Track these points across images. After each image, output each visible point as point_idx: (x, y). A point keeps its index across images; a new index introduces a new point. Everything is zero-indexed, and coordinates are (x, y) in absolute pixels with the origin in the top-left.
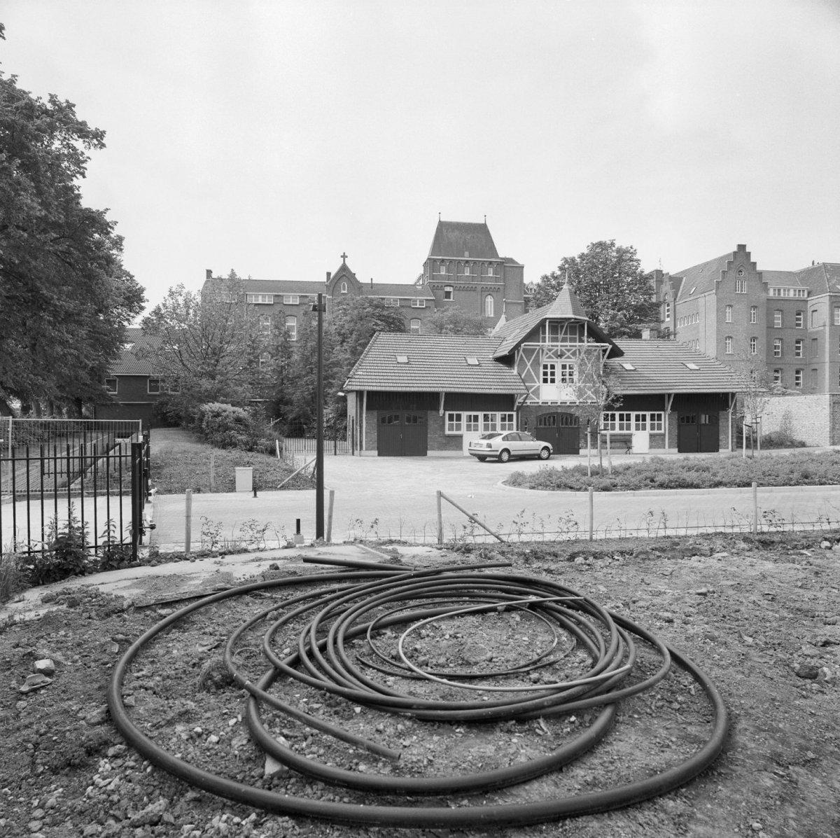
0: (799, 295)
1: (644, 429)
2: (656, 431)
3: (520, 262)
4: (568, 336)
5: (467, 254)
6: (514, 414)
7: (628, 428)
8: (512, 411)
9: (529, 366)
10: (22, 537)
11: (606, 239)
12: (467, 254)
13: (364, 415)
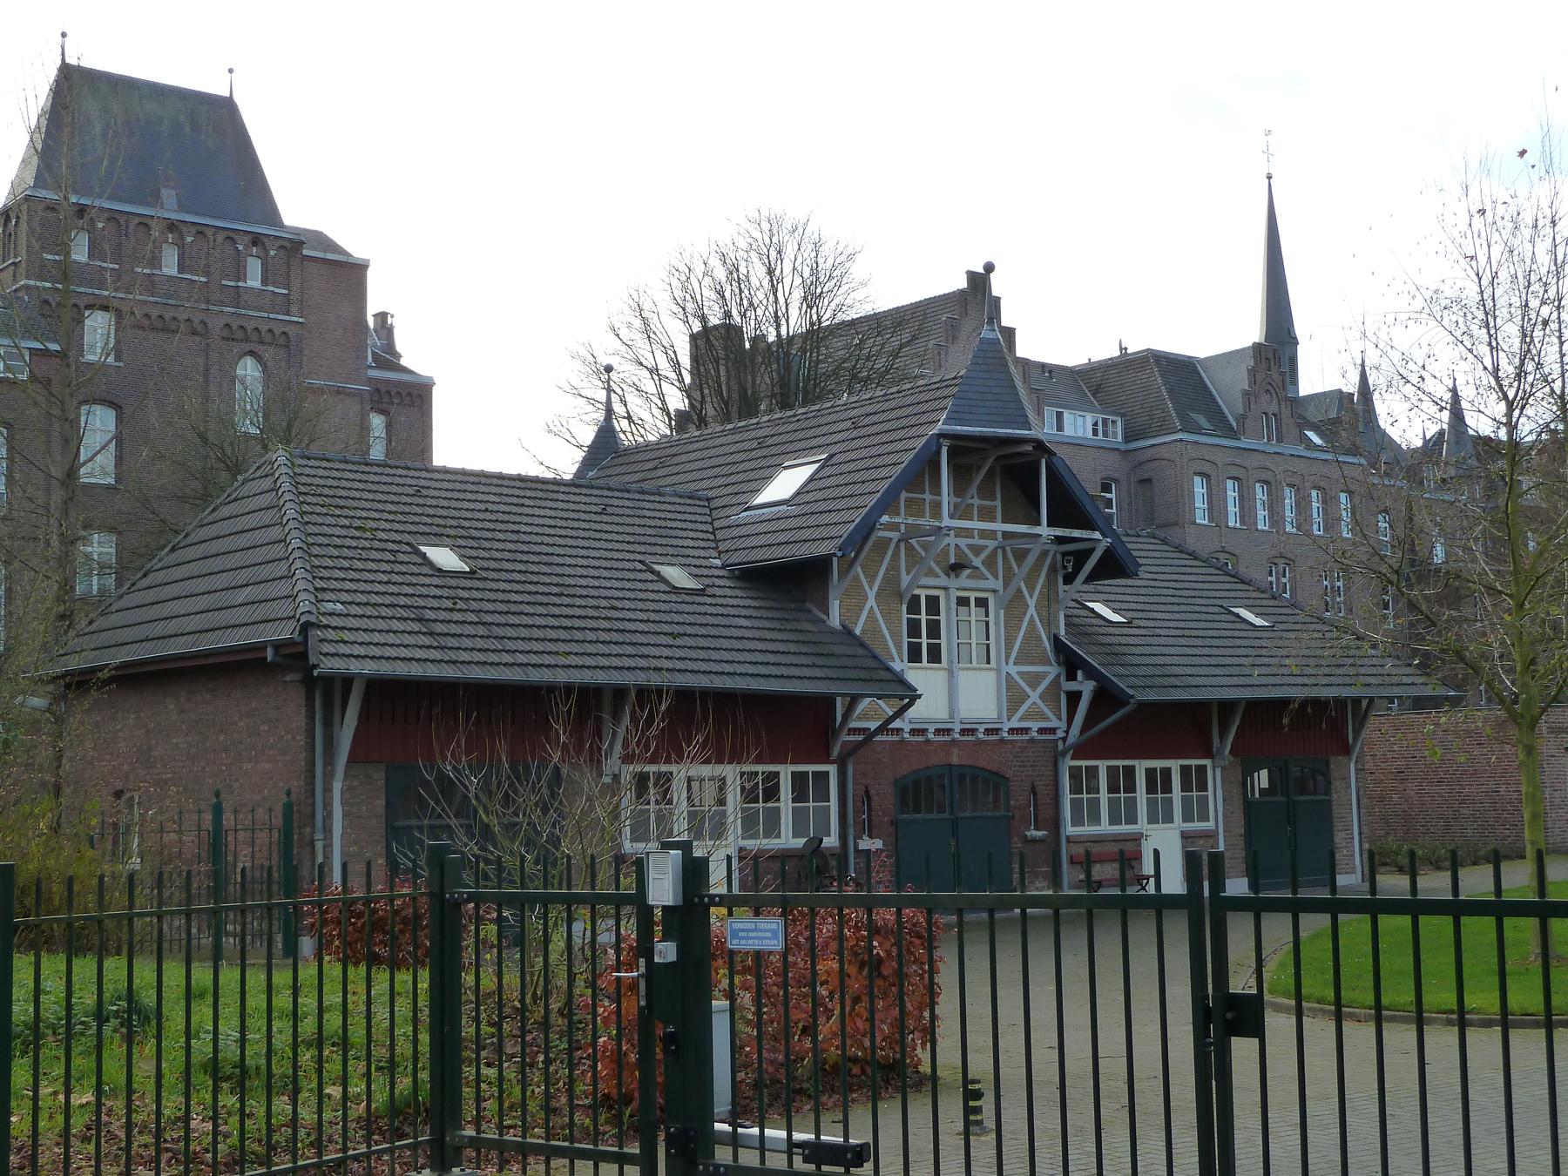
0: (1105, 434)
1: (1169, 819)
3: (355, 247)
4: (976, 502)
5: (169, 196)
6: (832, 769)
7: (1132, 819)
8: (826, 760)
9: (871, 602)
10: (1075, 964)
11: (793, 213)
12: (169, 196)
13: (337, 787)
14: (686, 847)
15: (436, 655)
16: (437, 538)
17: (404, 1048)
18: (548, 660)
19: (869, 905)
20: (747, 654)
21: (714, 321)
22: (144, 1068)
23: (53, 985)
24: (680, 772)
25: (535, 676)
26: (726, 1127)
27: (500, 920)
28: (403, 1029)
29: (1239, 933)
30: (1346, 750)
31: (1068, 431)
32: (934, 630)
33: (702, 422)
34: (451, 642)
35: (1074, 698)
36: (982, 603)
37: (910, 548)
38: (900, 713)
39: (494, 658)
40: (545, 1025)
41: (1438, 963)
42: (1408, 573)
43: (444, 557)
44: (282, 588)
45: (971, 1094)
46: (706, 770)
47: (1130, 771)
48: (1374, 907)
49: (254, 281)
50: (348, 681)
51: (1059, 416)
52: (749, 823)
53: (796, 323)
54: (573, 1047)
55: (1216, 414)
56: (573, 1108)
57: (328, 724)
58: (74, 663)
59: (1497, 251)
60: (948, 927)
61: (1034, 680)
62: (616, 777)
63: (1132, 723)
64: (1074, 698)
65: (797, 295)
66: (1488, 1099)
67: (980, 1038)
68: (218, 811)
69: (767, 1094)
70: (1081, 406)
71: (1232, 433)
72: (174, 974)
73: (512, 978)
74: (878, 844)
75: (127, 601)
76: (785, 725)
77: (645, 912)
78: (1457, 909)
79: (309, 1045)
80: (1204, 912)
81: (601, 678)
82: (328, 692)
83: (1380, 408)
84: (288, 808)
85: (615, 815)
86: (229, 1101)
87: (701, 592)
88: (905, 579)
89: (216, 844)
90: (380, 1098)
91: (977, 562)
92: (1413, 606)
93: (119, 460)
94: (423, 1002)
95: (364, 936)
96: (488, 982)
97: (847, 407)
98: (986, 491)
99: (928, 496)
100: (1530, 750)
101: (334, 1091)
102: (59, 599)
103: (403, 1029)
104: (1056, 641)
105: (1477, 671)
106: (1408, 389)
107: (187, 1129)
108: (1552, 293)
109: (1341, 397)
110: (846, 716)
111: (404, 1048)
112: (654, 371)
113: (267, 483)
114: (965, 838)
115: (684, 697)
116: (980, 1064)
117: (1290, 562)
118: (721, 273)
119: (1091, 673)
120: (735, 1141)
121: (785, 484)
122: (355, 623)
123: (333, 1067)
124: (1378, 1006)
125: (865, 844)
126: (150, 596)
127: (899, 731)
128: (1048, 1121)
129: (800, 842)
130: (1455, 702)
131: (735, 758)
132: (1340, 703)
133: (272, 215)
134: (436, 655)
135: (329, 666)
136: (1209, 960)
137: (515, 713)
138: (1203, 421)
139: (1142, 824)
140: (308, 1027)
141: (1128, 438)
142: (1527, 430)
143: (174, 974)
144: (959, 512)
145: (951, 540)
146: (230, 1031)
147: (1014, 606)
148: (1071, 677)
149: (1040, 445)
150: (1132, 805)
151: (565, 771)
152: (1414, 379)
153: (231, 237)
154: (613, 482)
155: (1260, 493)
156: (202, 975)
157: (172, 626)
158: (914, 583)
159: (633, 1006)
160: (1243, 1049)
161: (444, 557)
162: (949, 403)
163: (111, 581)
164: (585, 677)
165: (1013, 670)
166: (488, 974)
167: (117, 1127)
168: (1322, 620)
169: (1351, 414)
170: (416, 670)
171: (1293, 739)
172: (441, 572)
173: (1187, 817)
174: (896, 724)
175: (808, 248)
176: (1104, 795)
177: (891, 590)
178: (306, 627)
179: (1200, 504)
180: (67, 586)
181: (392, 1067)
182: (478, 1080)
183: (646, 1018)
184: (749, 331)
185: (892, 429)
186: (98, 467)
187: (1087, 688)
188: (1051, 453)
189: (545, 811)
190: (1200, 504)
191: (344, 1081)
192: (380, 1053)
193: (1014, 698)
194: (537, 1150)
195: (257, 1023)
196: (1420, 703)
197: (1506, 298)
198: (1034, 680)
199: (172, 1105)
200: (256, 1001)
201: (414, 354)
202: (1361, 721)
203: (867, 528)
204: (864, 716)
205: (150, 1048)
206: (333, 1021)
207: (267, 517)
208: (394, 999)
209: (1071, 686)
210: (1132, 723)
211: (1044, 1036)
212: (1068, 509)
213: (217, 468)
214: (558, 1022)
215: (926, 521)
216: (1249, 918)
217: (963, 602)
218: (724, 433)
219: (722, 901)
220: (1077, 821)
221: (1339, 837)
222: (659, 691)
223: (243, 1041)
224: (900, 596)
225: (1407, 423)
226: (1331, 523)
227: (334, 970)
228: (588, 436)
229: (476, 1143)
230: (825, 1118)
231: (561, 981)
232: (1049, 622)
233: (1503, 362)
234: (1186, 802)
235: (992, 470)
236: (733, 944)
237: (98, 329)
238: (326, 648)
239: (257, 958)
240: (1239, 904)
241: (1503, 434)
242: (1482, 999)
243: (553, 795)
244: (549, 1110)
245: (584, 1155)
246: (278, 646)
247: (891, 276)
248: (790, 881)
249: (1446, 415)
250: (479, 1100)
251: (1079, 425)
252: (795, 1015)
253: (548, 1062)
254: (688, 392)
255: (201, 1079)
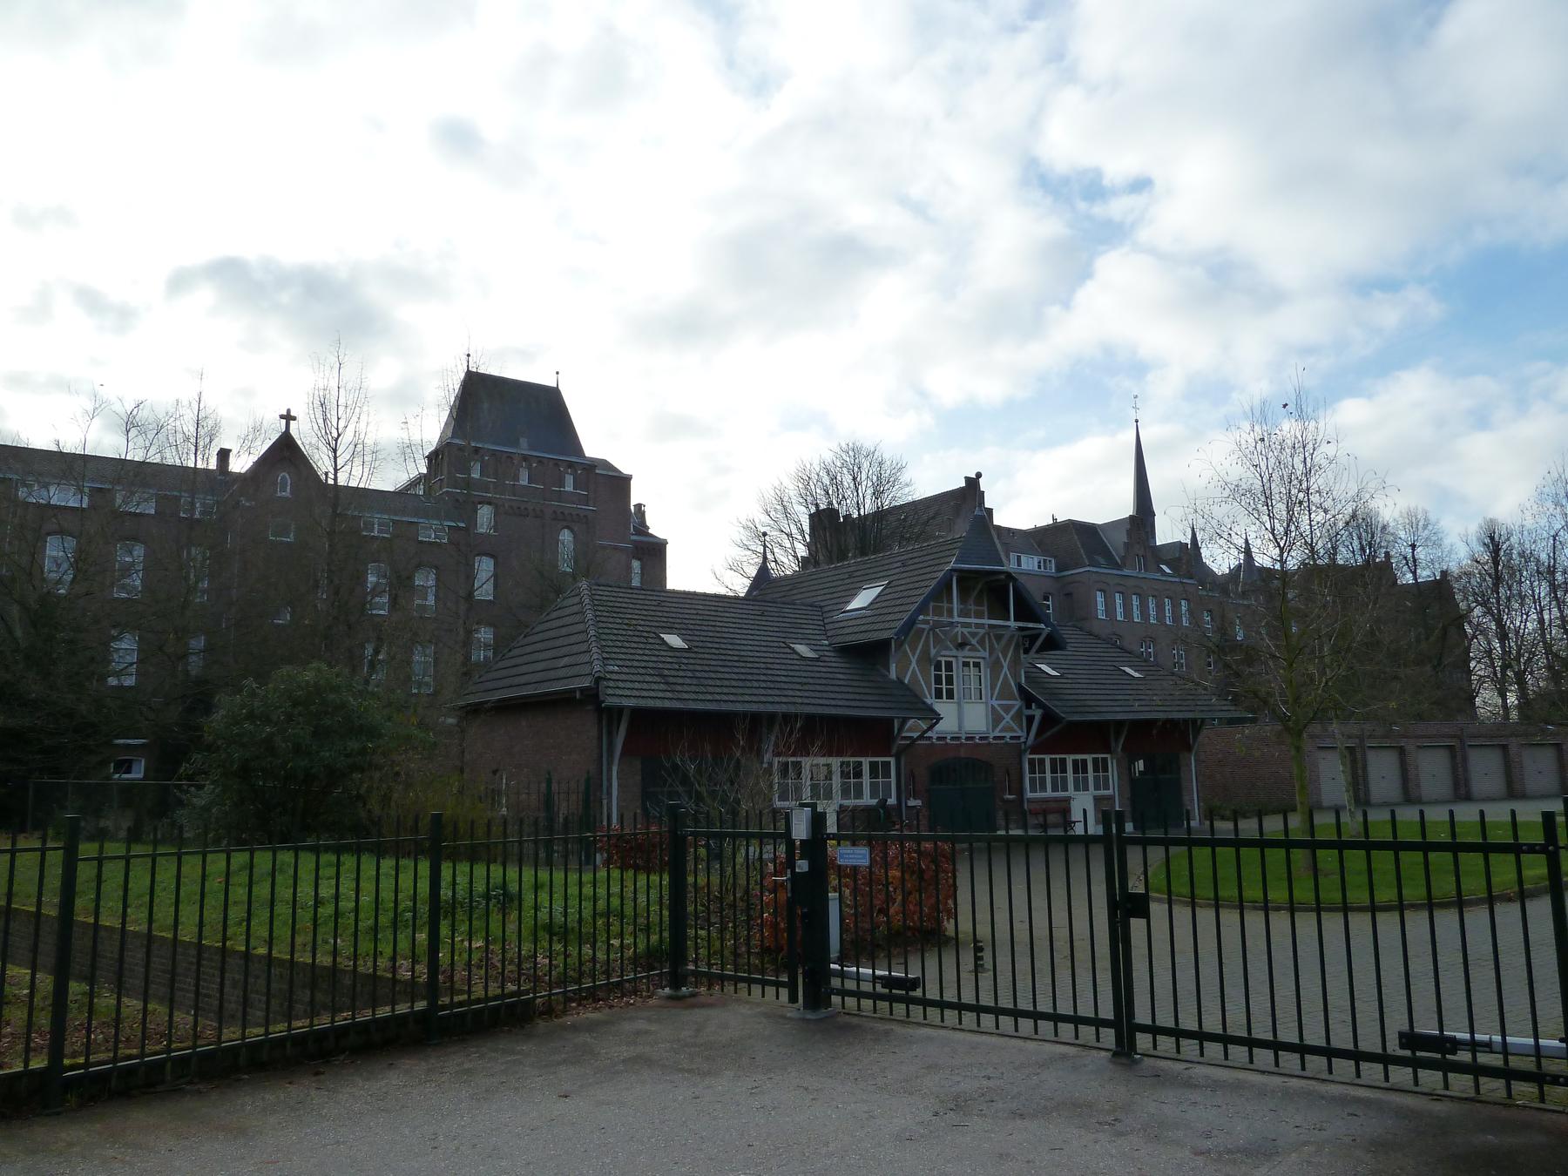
2: (1102, 792)
4: (973, 607)
6: (892, 760)
9: (914, 664)
10: (1038, 874)
11: (868, 445)
12: (523, 442)
13: (615, 769)
14: (813, 806)
15: (669, 695)
16: (670, 630)
17: (654, 918)
18: (732, 698)
19: (918, 840)
20: (844, 696)
21: (822, 507)
22: (512, 927)
23: (462, 880)
24: (807, 762)
25: (724, 707)
26: (836, 967)
27: (707, 846)
28: (654, 908)
29: (1134, 856)
30: (1189, 749)
31: (1024, 566)
32: (950, 680)
33: (817, 564)
34: (679, 688)
35: (1030, 719)
36: (977, 665)
37: (936, 636)
38: (931, 728)
39: (701, 697)
40: (733, 906)
41: (1227, 871)
42: (1224, 646)
43: (674, 640)
44: (585, 658)
45: (978, 949)
46: (822, 760)
47: (1063, 761)
48: (1213, 843)
49: (569, 487)
50: (621, 710)
51: (1019, 558)
52: (845, 793)
53: (869, 507)
54: (749, 918)
55: (1107, 553)
56: (749, 953)
57: (610, 733)
58: (472, 699)
59: (1272, 461)
60: (963, 850)
61: (1007, 709)
62: (771, 764)
63: (1063, 733)
64: (1030, 719)
65: (870, 491)
66: (1282, 957)
67: (983, 915)
68: (549, 782)
69: (856, 950)
70: (1030, 551)
71: (1118, 567)
72: (528, 874)
73: (715, 879)
74: (918, 803)
75: (500, 665)
76: (862, 735)
77: (791, 844)
78: (1263, 844)
79: (601, 915)
80: (1113, 845)
81: (762, 708)
82: (612, 715)
83: (1204, 552)
84: (588, 781)
85: (771, 786)
86: (558, 947)
87: (817, 660)
88: (933, 652)
89: (548, 802)
90: (641, 946)
91: (974, 642)
92: (1227, 666)
93: (496, 587)
94: (666, 893)
95: (631, 854)
96: (702, 881)
97: (899, 554)
98: (978, 602)
99: (946, 605)
100: (1298, 749)
101: (615, 942)
102: (464, 664)
103: (654, 908)
104: (1020, 687)
105: (1265, 702)
106: (1222, 542)
107: (536, 964)
108: (1304, 486)
109: (1180, 546)
110: (900, 729)
111: (654, 918)
112: (789, 535)
113: (576, 600)
114: (968, 802)
115: (810, 719)
116: (983, 931)
117: (1153, 640)
118: (826, 480)
119: (1040, 705)
120: (842, 975)
121: (862, 600)
122: (624, 677)
123: (615, 929)
124: (1217, 898)
125: (912, 803)
126: (513, 662)
127: (930, 738)
128: (1023, 964)
129: (874, 802)
130: (1254, 721)
131: (839, 754)
132: (1185, 721)
133: (576, 447)
134: (669, 695)
135: (611, 701)
136: (1116, 874)
137: (719, 731)
138: (1102, 561)
139: (1071, 792)
140: (601, 904)
141: (1058, 569)
142: (1292, 564)
143: (528, 874)
144: (963, 614)
145: (959, 629)
146: (558, 907)
147: (995, 667)
148: (1029, 707)
149: (1009, 575)
150: (1064, 780)
151: (743, 761)
152: (1225, 535)
153: (557, 463)
154: (768, 598)
155: (1135, 601)
156: (544, 875)
157: (523, 680)
158: (938, 654)
159: (783, 896)
160: (1137, 925)
161: (674, 640)
162: (957, 552)
163: (490, 654)
164: (754, 708)
165: (995, 703)
166: (700, 877)
167: (496, 960)
168: (1173, 674)
169: (1187, 556)
170: (658, 704)
171: (1156, 744)
172: (672, 649)
173: (1097, 788)
174: (929, 734)
175: (876, 469)
176: (1048, 775)
177: (925, 659)
178: (598, 680)
179: (1101, 607)
180: (467, 657)
181: (648, 929)
182: (696, 937)
183: (791, 904)
184: (842, 512)
185: (911, 562)
186: (484, 590)
187: (1038, 713)
188: (1015, 580)
189: (732, 783)
190: (1101, 607)
191: (621, 936)
192: (641, 920)
193: (996, 719)
194: (729, 978)
195: (573, 902)
196: (1232, 722)
197: (1277, 489)
198: (1007, 709)
199: (527, 948)
200: (573, 890)
201: (656, 527)
202: (1197, 731)
203: (911, 623)
204: (910, 730)
205: (514, 915)
206: (615, 902)
207: (577, 618)
208: (647, 891)
209: (1029, 712)
210: (1063, 733)
211: (1021, 913)
212: (1026, 611)
213: (551, 589)
214: (741, 905)
215: (945, 619)
216: (1061, 848)
217: (966, 664)
218: (830, 570)
219: (834, 837)
220: (1033, 790)
221: (1186, 798)
222: (796, 715)
223: (566, 916)
224: (929, 660)
225: (1220, 560)
226: (1176, 617)
227: (616, 874)
228: (753, 571)
229: (696, 974)
230: (893, 962)
231: (742, 881)
232: (1016, 676)
233: (1277, 525)
234: (1096, 779)
235: (981, 591)
236: (840, 862)
237: (485, 515)
238: (610, 691)
239: (574, 865)
240: (1134, 841)
241: (1278, 566)
242: (1278, 894)
243: (737, 775)
244: (736, 955)
245: (756, 981)
246: (582, 690)
247: (927, 479)
248: (868, 824)
249: (1242, 556)
250: (697, 949)
251: (1030, 563)
252: (877, 902)
253: (735, 927)
254: (808, 546)
255: (542, 934)
